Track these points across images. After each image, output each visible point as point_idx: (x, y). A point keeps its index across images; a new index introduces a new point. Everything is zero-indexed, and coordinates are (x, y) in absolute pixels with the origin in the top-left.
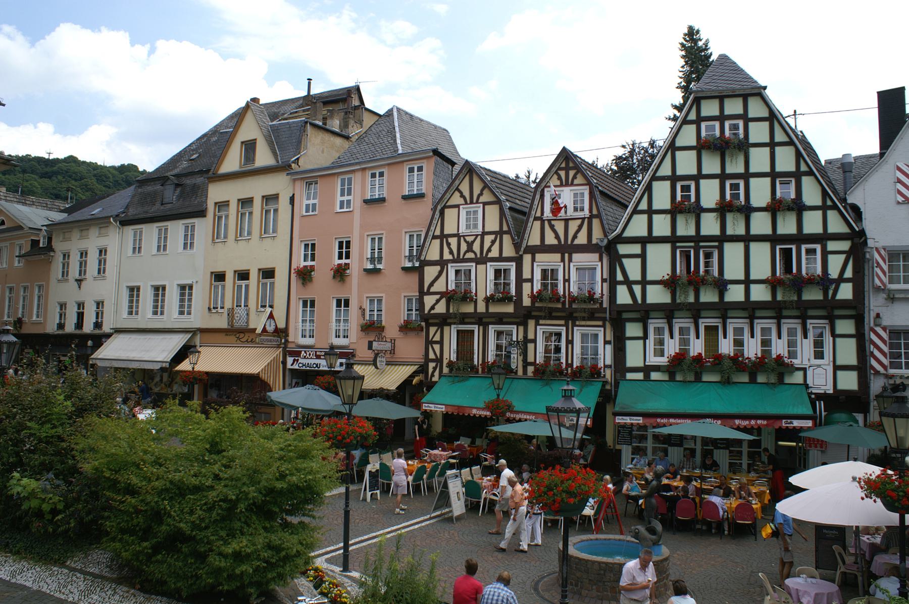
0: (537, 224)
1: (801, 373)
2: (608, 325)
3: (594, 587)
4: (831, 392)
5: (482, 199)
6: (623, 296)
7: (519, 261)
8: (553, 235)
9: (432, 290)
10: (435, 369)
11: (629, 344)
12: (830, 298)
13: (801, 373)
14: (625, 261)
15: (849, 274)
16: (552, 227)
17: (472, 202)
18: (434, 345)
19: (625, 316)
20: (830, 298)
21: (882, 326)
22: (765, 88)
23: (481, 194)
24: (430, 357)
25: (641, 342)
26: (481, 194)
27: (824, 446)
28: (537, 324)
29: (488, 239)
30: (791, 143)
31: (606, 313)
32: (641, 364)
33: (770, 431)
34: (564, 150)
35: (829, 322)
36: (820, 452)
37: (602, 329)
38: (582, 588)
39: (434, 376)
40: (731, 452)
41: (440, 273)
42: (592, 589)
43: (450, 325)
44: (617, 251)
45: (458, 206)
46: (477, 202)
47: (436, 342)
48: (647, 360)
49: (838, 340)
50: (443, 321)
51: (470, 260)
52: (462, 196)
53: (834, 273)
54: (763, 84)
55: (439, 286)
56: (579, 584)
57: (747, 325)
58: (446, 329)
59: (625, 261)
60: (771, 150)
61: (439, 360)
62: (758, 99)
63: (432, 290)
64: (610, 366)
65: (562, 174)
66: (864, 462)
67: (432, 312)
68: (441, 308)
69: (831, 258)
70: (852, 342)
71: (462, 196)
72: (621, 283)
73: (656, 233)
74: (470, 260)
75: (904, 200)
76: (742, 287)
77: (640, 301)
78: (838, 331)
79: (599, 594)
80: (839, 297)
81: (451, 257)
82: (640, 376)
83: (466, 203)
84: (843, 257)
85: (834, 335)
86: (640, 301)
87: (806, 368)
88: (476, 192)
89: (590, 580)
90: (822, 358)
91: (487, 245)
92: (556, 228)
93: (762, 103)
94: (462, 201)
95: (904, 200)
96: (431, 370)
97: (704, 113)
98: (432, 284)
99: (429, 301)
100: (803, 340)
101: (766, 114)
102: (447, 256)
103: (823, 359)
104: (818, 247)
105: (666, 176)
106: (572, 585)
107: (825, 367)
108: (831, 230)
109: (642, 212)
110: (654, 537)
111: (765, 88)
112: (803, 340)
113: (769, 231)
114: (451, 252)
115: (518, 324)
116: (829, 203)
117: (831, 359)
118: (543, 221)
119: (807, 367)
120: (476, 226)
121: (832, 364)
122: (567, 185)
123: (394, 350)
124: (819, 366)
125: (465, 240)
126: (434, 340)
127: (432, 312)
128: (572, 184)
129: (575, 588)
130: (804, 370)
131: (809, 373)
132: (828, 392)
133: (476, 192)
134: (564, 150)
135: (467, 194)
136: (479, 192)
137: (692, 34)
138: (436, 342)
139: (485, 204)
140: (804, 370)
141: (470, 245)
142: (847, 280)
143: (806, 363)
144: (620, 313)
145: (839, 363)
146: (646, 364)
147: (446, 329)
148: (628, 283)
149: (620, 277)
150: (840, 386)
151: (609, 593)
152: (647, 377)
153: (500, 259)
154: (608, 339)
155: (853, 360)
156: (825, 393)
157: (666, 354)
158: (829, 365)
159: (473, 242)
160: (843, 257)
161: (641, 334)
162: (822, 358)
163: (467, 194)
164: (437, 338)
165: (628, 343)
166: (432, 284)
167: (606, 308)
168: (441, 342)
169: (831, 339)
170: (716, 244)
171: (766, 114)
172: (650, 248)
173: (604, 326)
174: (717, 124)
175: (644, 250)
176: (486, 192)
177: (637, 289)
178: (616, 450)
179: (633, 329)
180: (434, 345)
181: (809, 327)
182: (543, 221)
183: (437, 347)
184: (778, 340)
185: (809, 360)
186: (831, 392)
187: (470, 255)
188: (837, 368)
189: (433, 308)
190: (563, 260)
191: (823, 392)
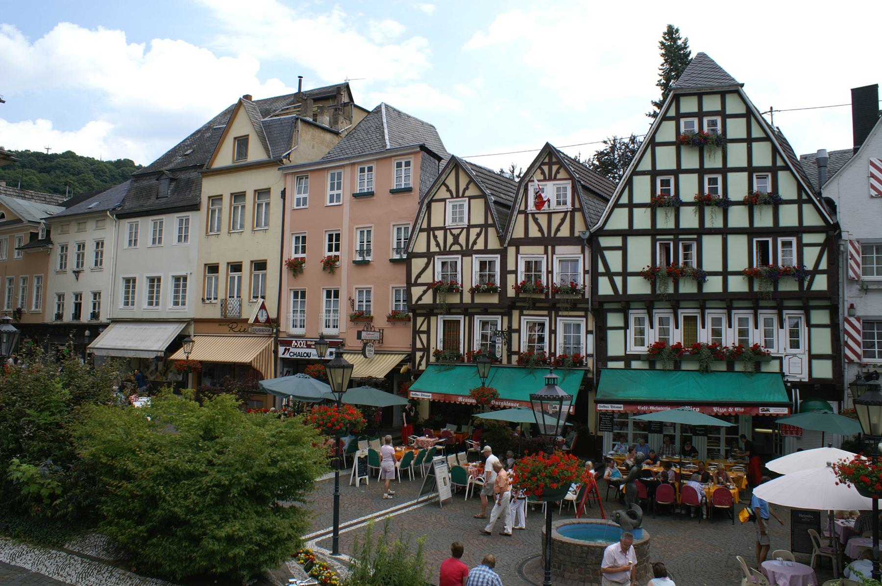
0: (521, 217)
1: (777, 362)
2: (590, 315)
3: (577, 570)
4: (807, 380)
5: (468, 193)
6: (605, 288)
7: (503, 253)
8: (536, 228)
9: (419, 281)
10: (422, 358)
11: (610, 333)
12: (805, 289)
13: (777, 362)
14: (606, 253)
15: (823, 265)
16: (536, 220)
17: (458, 196)
18: (421, 335)
19: (606, 306)
20: (805, 289)
21: (856, 316)
22: (742, 85)
23: (467, 188)
24: (417, 347)
25: (622, 331)
26: (467, 188)
27: (800, 433)
28: (521, 314)
29: (474, 232)
30: (767, 139)
31: (588, 303)
32: (622, 354)
33: (747, 418)
34: (547, 145)
35: (805, 312)
36: (795, 439)
37: (584, 319)
38: (564, 570)
39: (421, 365)
40: (709, 438)
41: (427, 265)
42: (575, 572)
43: (436, 315)
44: (599, 244)
45: (444, 200)
46: (463, 196)
47: (423, 332)
48: (628, 349)
49: (813, 330)
50: (430, 312)
51: (456, 252)
52: (448, 190)
53: (809, 265)
54: (741, 82)
55: (426, 278)
56: (562, 566)
57: (725, 315)
58: (433, 319)
59: (606, 253)
60: (748, 145)
61: (426, 350)
62: (736, 96)
63: (419, 281)
64: (592, 356)
65: (546, 168)
66: (838, 448)
67: (420, 302)
68: (428, 299)
69: (806, 250)
70: (827, 332)
71: (448, 190)
72: (602, 274)
73: (636, 226)
74: (456, 252)
75: (877, 194)
76: (720, 279)
77: (621, 292)
78: (814, 321)
79: (581, 576)
80: (814, 288)
81: (437, 250)
82: (621, 365)
83: (452, 197)
84: (818, 249)
85: (809, 325)
86: (621, 292)
87: (782, 357)
88: (462, 186)
89: (572, 563)
90: (798, 347)
91: (472, 237)
92: (539, 221)
93: (740, 100)
94: (448, 195)
95: (877, 194)
96: (418, 359)
97: (684, 109)
98: (419, 276)
99: (416, 292)
100: (779, 329)
101: (743, 111)
102: (434, 248)
103: (799, 348)
104: (794, 240)
105: (646, 171)
106: (555, 568)
107: (800, 356)
108: (806, 223)
109: (623, 206)
110: (634, 521)
111: (742, 85)
112: (779, 329)
113: (746, 224)
114: (438, 245)
115: (502, 315)
116: (804, 197)
117: (807, 348)
118: (527, 215)
119: (783, 356)
120: (461, 219)
121: (807, 353)
122: (550, 179)
123: (382, 339)
124: (795, 355)
125: (451, 233)
126: (421, 330)
127: (420, 302)
128: (555, 179)
129: (558, 571)
130: (780, 359)
131: (785, 362)
132: (803, 380)
133: (462, 186)
134: (547, 145)
135: (453, 188)
136: (465, 186)
137: (671, 33)
138: (423, 332)
139: (470, 198)
140: (780, 359)
141: (456, 238)
142: (822, 272)
143: (782, 353)
144: (601, 304)
145: (814, 352)
146: (627, 353)
147: (433, 319)
148: (610, 274)
149: (601, 269)
150: (815, 375)
151: (591, 576)
152: (628, 366)
153: (486, 251)
154: (590, 328)
155: (827, 350)
156: (801, 382)
157: (646, 344)
158: (804, 354)
159: (459, 235)
160: (818, 249)
161: (622, 324)
162: (798, 347)
163: (453, 188)
164: (424, 328)
165: (610, 333)
166: (419, 276)
167: (588, 299)
168: (428, 332)
169: (807, 328)
170: (695, 237)
171: (743, 111)
172: (631, 240)
173: (586, 316)
174: (696, 121)
175: (625, 243)
176: (471, 186)
177: (618, 280)
178: (598, 436)
179: (614, 320)
180: (421, 335)
181: (785, 317)
182: (527, 215)
183: (424, 337)
184: (755, 330)
185: (785, 349)
186: (807, 380)
187: (456, 248)
188: (812, 357)
189: (420, 299)
190: (546, 252)
191: (798, 380)
